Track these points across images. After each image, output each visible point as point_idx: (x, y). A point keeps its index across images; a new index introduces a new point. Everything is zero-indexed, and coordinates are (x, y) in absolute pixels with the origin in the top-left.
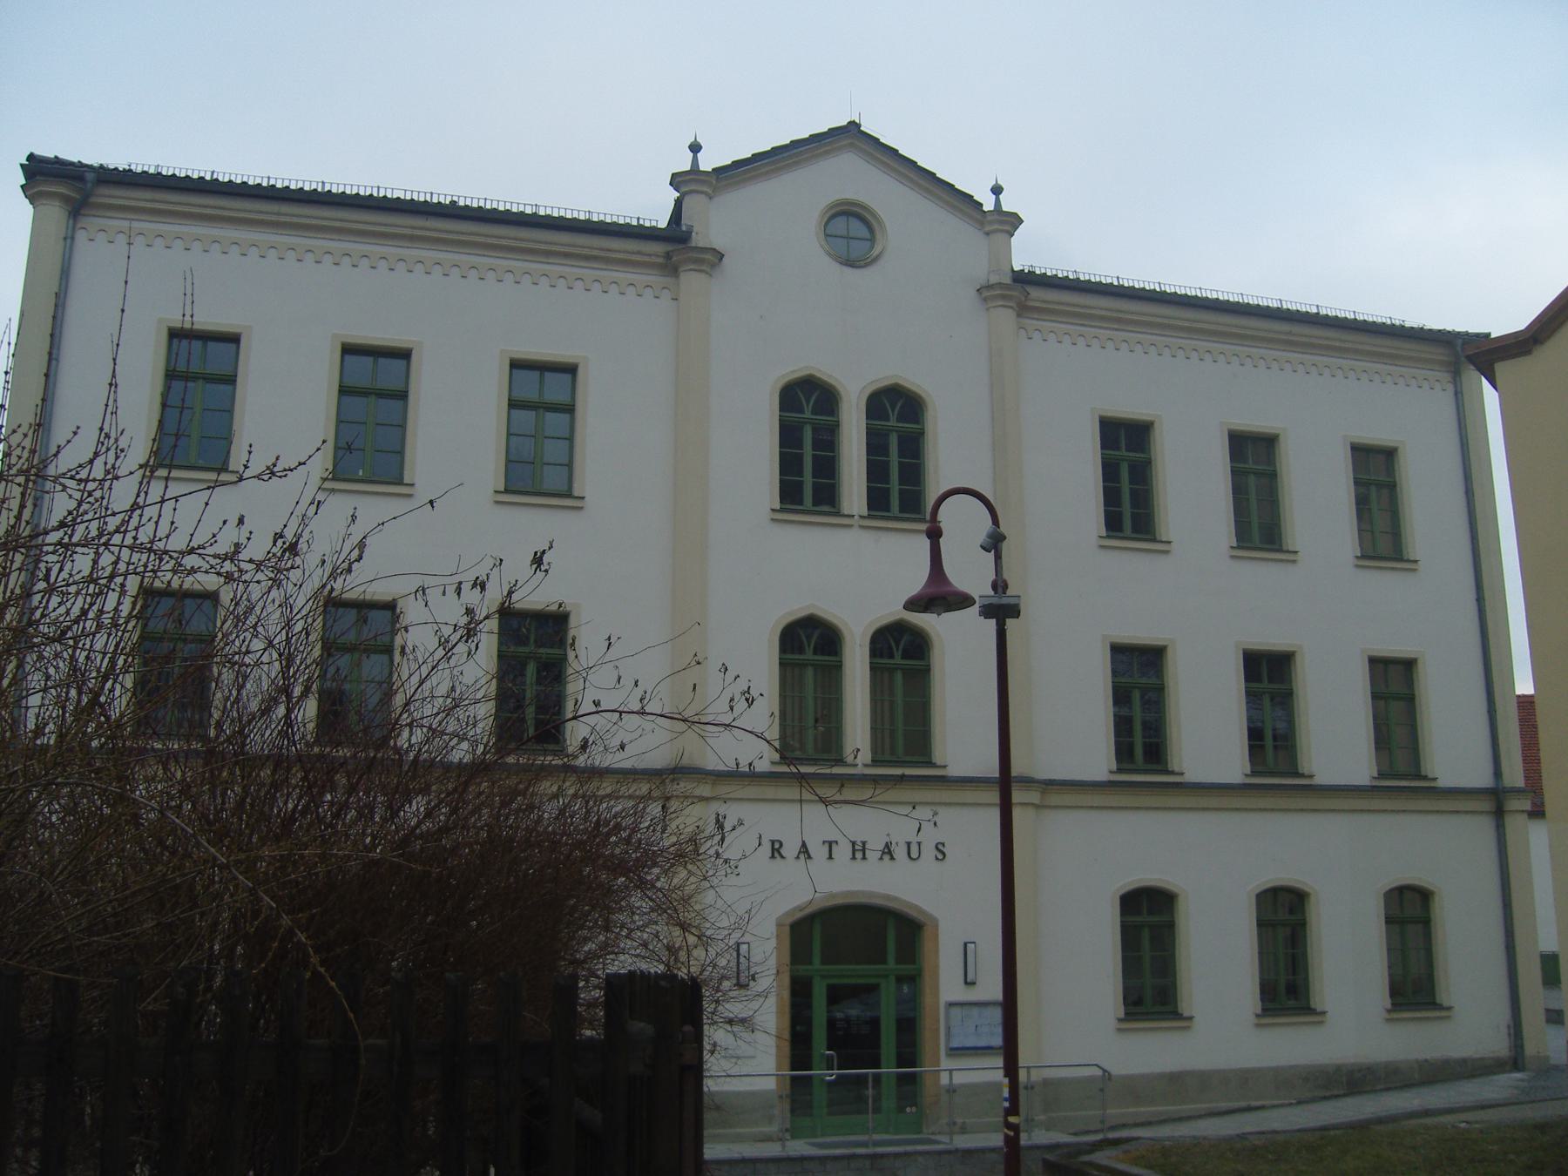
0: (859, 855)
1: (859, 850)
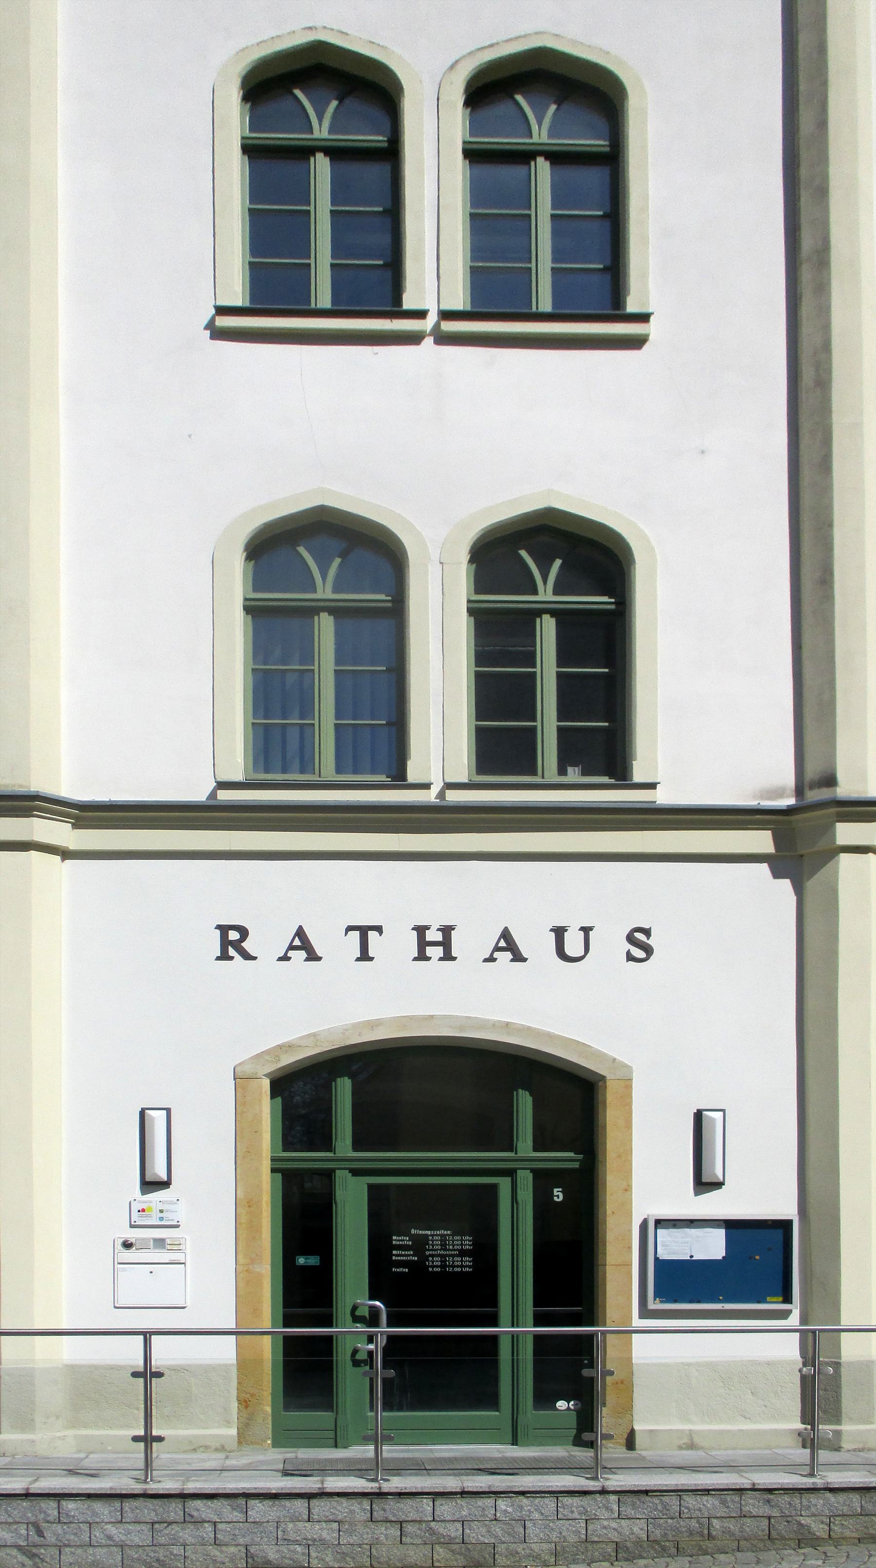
0: (435, 952)
1: (434, 943)
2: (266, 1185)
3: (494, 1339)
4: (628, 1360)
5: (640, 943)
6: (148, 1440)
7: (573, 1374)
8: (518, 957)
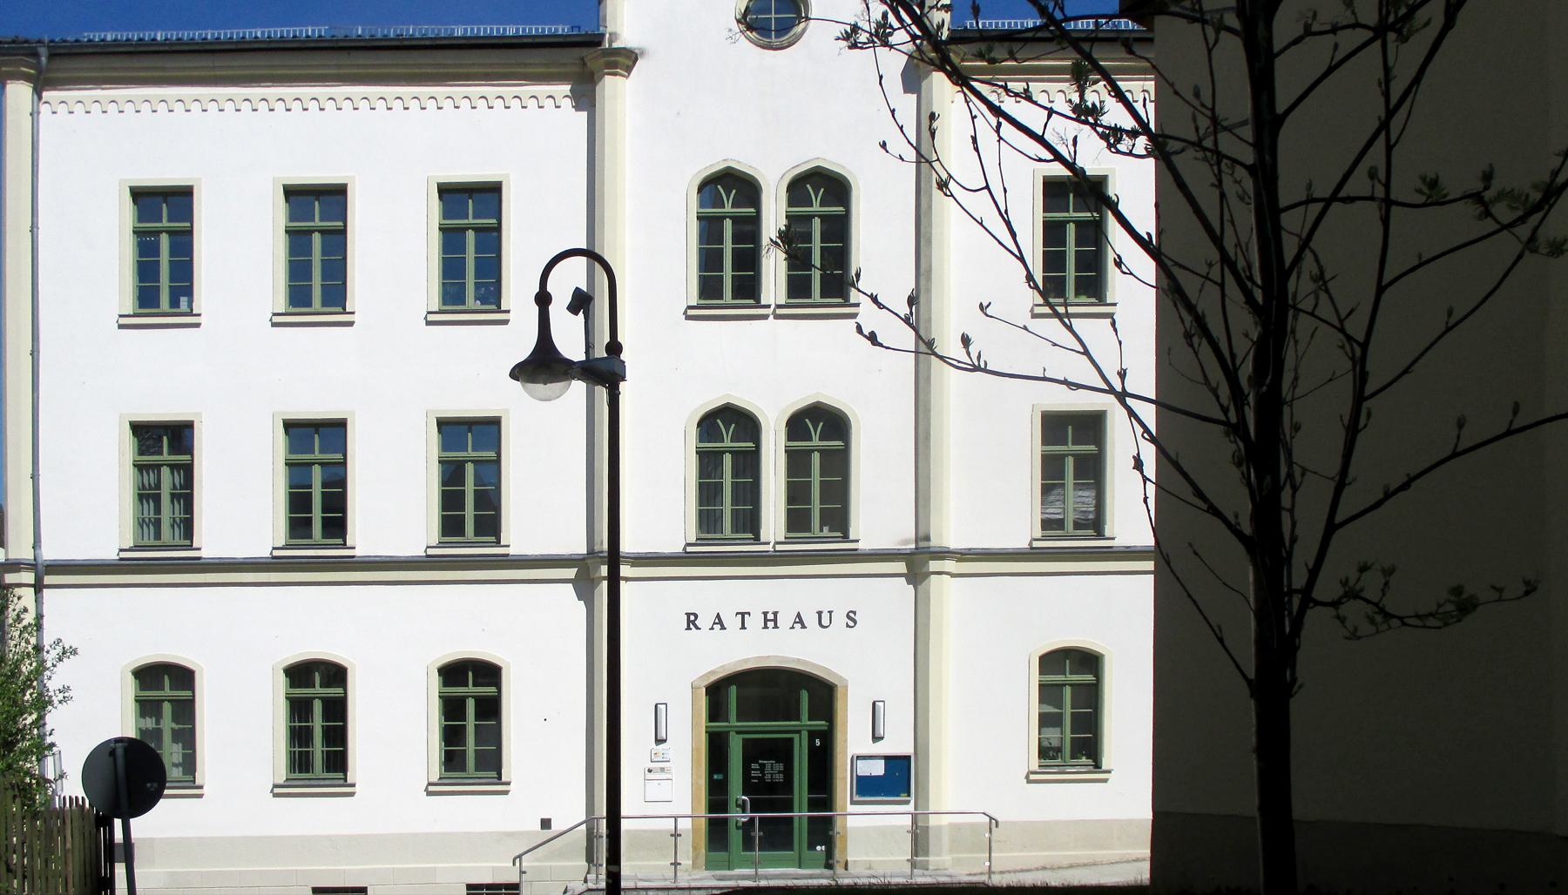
0: (771, 624)
1: (771, 620)
2: (703, 738)
3: (791, 818)
4: (845, 827)
5: (851, 617)
6: (676, 864)
7: (823, 832)
8: (803, 627)
